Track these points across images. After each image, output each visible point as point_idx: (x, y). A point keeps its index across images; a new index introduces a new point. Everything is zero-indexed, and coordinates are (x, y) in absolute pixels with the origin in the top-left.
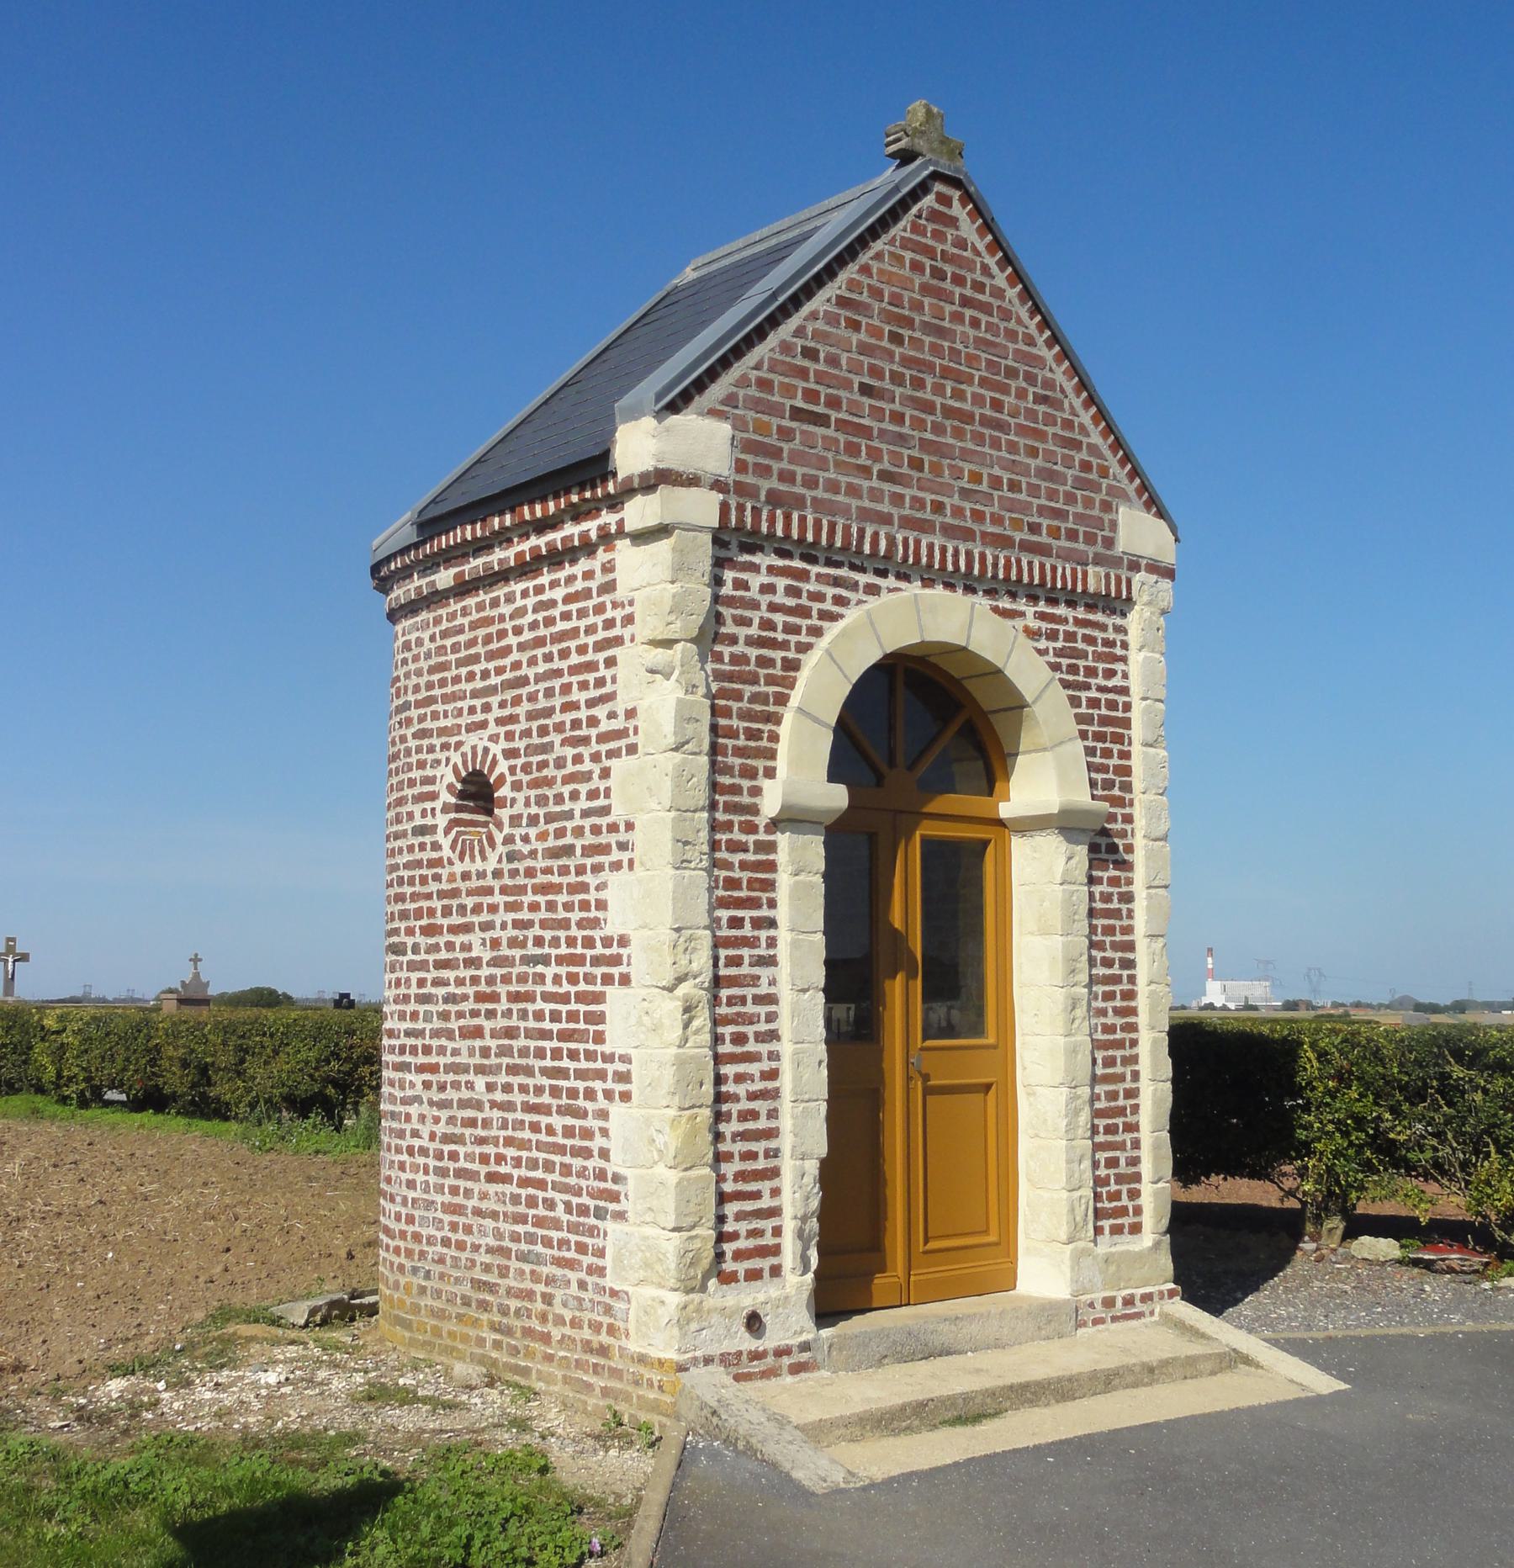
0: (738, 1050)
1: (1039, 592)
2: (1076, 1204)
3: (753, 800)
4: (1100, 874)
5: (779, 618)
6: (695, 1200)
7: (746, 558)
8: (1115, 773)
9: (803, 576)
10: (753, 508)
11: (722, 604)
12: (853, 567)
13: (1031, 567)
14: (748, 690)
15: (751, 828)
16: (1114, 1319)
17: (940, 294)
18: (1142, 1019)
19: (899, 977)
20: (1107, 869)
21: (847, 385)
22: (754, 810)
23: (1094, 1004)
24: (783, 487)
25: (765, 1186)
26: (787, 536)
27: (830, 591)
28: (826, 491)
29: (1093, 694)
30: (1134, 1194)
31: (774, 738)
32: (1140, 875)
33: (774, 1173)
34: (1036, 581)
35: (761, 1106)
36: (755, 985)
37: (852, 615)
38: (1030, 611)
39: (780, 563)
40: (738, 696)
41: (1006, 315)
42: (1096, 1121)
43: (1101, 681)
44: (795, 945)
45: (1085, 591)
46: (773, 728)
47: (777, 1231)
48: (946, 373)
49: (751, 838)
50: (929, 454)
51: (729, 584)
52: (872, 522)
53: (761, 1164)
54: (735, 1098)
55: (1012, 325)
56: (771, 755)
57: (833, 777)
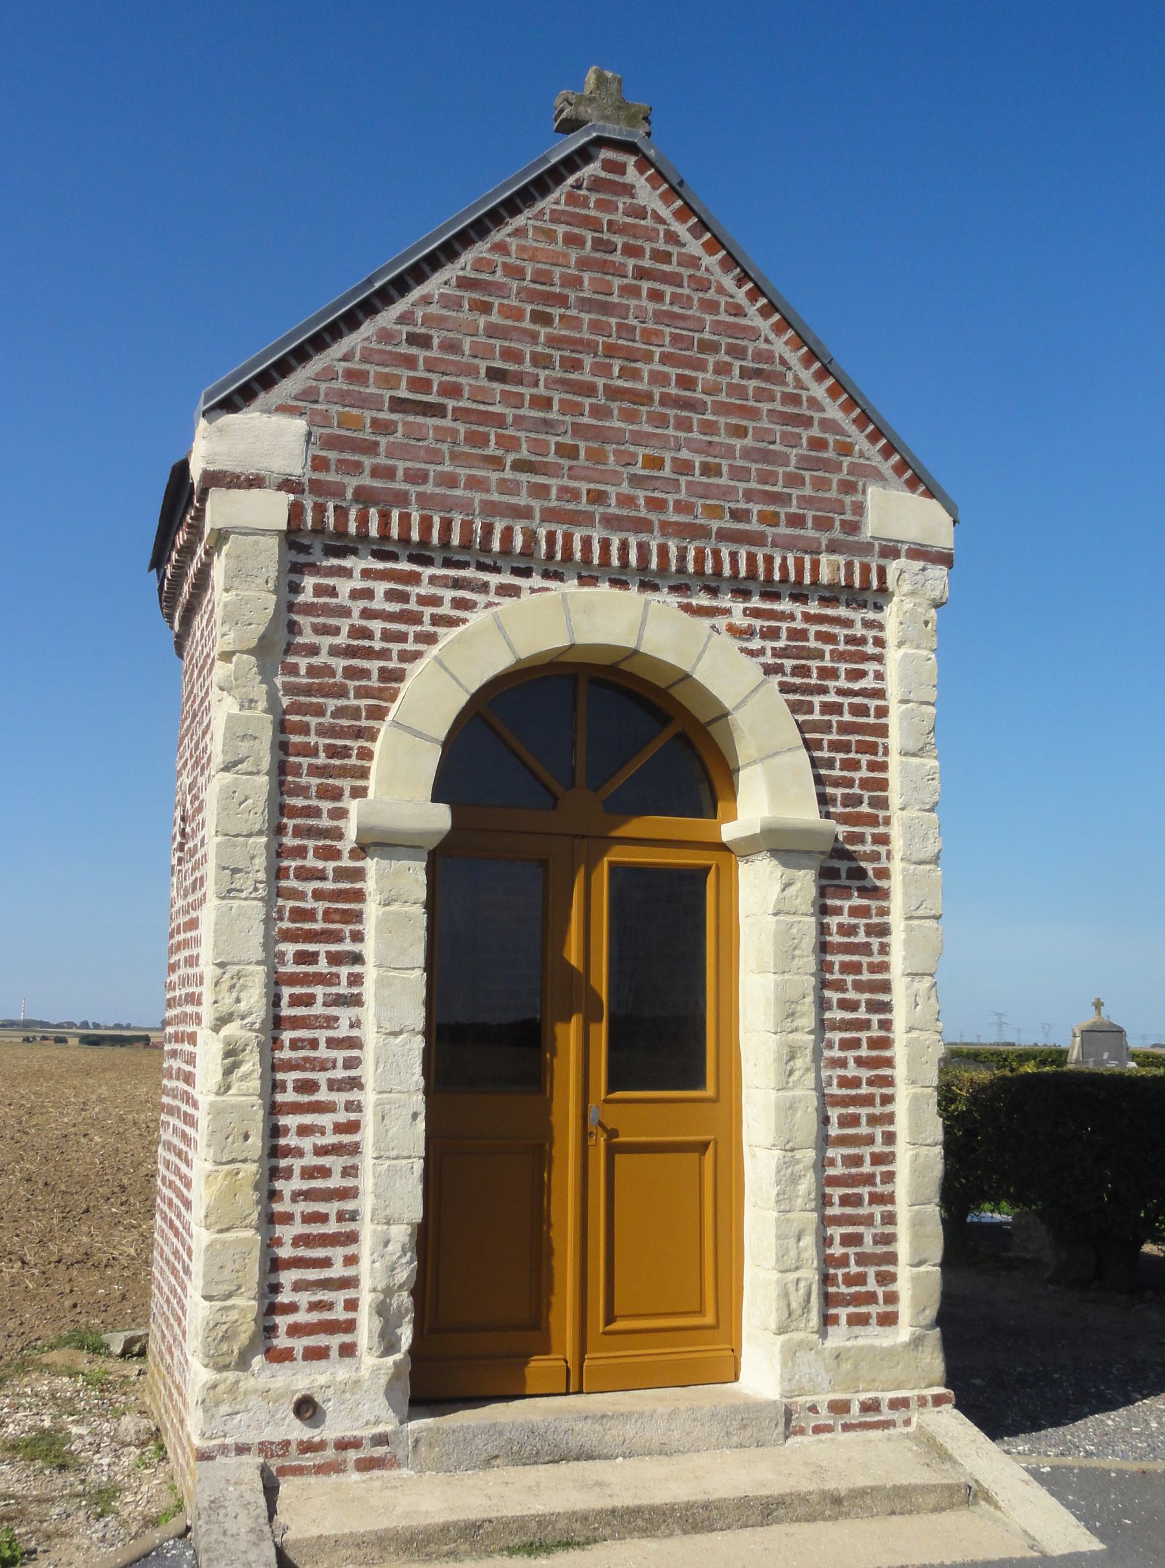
0: (305, 1098)
1: (751, 586)
2: (791, 1288)
3: (335, 823)
4: (838, 903)
5: (376, 626)
6: (230, 1266)
7: (334, 562)
8: (861, 787)
9: (415, 578)
10: (336, 508)
11: (298, 613)
12: (481, 567)
13: (735, 558)
14: (332, 704)
15: (335, 854)
16: (846, 1427)
17: (604, 267)
18: (900, 1072)
19: (574, 1019)
20: (849, 897)
21: (472, 371)
22: (339, 835)
23: (827, 1053)
24: (377, 484)
25: (337, 1253)
26: (385, 536)
27: (448, 594)
28: (436, 485)
29: (832, 698)
30: (886, 1278)
31: (366, 754)
32: (897, 904)
33: (352, 1238)
34: (743, 573)
35: (334, 1162)
36: (329, 1027)
37: (476, 618)
38: (738, 607)
39: (380, 565)
40: (319, 711)
41: (702, 285)
42: (828, 1190)
43: (842, 683)
44: (381, 982)
45: (815, 582)
46: (366, 744)
47: (352, 1305)
48: (611, 351)
49: (331, 865)
50: (586, 439)
51: (309, 590)
52: (502, 516)
53: (332, 1227)
54: (299, 1153)
55: (711, 295)
56: (364, 773)
57: (436, 797)
